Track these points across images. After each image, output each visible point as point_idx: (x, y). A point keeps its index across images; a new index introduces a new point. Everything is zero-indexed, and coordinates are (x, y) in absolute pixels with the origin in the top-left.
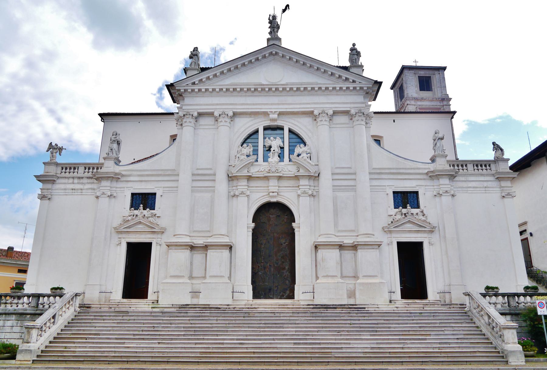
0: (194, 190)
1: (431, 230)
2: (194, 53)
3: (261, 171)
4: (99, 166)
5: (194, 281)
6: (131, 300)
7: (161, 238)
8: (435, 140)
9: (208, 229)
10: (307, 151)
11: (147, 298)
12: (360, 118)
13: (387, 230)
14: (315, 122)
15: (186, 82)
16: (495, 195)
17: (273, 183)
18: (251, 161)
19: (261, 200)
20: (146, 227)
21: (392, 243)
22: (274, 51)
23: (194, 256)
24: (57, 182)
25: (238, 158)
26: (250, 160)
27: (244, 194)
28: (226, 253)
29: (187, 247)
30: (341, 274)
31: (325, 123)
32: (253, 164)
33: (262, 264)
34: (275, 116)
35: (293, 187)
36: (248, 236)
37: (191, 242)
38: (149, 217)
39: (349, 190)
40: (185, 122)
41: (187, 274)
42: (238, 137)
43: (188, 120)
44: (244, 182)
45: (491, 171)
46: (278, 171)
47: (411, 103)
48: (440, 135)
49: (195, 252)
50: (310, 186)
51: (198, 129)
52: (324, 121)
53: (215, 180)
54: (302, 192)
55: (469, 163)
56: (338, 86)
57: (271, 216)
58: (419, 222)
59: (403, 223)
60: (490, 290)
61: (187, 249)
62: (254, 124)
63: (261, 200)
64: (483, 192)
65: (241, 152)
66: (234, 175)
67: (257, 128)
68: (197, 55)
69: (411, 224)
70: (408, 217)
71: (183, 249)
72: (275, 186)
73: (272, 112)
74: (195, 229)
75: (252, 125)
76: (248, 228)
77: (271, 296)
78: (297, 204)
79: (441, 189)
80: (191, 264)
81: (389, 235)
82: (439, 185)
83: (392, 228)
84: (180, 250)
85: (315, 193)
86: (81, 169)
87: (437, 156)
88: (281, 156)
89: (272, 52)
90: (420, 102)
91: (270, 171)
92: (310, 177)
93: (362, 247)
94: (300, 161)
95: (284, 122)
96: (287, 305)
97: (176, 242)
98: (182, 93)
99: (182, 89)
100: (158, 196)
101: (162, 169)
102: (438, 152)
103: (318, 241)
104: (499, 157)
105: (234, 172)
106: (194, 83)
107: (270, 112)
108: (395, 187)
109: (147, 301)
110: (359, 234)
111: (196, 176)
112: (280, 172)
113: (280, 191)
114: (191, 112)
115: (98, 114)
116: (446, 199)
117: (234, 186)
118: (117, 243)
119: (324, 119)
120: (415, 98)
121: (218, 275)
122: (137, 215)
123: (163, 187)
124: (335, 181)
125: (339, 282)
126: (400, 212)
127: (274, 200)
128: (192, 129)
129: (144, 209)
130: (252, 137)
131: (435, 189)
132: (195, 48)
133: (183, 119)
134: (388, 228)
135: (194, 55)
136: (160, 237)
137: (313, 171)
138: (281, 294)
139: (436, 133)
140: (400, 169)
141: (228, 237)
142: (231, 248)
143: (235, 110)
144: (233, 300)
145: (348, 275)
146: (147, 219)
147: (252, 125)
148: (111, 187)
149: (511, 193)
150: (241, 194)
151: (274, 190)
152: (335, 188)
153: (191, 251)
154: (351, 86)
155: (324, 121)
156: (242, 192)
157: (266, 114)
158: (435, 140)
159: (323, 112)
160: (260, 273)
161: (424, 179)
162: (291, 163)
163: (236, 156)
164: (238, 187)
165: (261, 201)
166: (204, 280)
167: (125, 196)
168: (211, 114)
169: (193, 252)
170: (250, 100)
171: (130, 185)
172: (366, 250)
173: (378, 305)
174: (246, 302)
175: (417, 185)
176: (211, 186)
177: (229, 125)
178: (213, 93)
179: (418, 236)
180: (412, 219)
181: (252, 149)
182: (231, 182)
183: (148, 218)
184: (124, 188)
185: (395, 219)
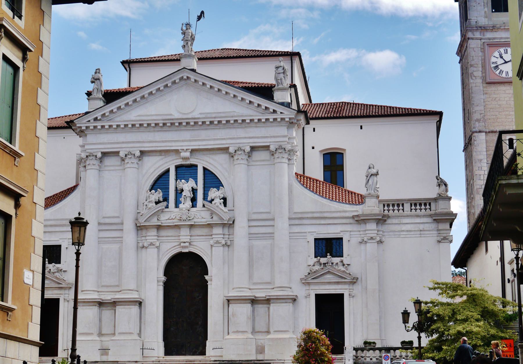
1: (352, 281)
3: (172, 219)
5: (103, 339)
6: (41, 358)
7: (69, 294)
8: (367, 177)
10: (220, 195)
11: (57, 356)
12: (281, 155)
13: (305, 282)
14: (232, 159)
18: (160, 208)
19: (172, 251)
20: (52, 282)
21: (309, 295)
23: (103, 312)
25: (146, 205)
27: (153, 245)
28: (135, 309)
29: (95, 304)
30: (253, 329)
31: (242, 162)
32: (164, 211)
33: (174, 319)
34: (188, 154)
35: (206, 236)
36: (159, 290)
37: (98, 299)
38: (55, 272)
39: (267, 238)
41: (95, 331)
42: (147, 180)
43: (92, 162)
45: (431, 211)
46: (190, 219)
47: (474, 35)
48: (374, 171)
49: (104, 308)
50: (224, 235)
51: (103, 170)
52: (241, 159)
53: (122, 230)
54: (215, 241)
55: (406, 202)
56: (256, 118)
57: (184, 267)
58: (339, 273)
59: (323, 274)
60: (367, 345)
61: (95, 306)
62: (165, 163)
63: (172, 251)
64: (418, 236)
65: (149, 199)
66: (142, 225)
67: (168, 168)
68: (99, 79)
69: (331, 275)
70: (328, 267)
71: (91, 306)
72: (187, 236)
73: (183, 149)
74: (103, 284)
75: (162, 165)
76: (158, 281)
77: (183, 353)
78: (210, 254)
79: (367, 235)
80: (100, 320)
81: (307, 288)
82: (365, 230)
83: (309, 280)
84: (88, 307)
85: (229, 243)
87: (367, 197)
88: (194, 200)
89: (183, 77)
90: (491, 33)
91: (181, 219)
92: (224, 225)
93: (274, 301)
94: (212, 207)
96: (194, 361)
97: (83, 299)
98: (84, 130)
99: (83, 126)
101: (66, 218)
102: (370, 191)
103: (229, 295)
104: (441, 194)
105: (142, 221)
106: (96, 119)
108: (317, 234)
109: (57, 358)
110: (275, 286)
112: (193, 219)
113: (192, 240)
114: (94, 152)
116: (371, 247)
117: (143, 236)
119: (240, 157)
120: (480, 27)
124: (251, 228)
125: (248, 338)
126: (318, 263)
127: (186, 250)
128: (96, 172)
130: (162, 177)
131: (361, 234)
133: (86, 160)
134: (305, 280)
135: (96, 79)
136: (68, 293)
137: (226, 218)
138: (194, 351)
139: (370, 168)
140: (324, 212)
141: (138, 293)
142: (140, 303)
143: (143, 149)
144: (143, 357)
146: (53, 274)
147: (162, 165)
149: (447, 238)
150: (150, 245)
151: (185, 241)
152: (252, 236)
153: (100, 307)
154: (271, 117)
155: (241, 157)
156: (151, 243)
157: (177, 152)
158: (367, 177)
160: (172, 329)
161: (350, 224)
162: (204, 209)
163: (143, 203)
164: (147, 238)
165: (173, 252)
169: (101, 308)
172: (279, 304)
173: (284, 360)
174: (157, 358)
176: (119, 236)
178: (117, 129)
179: (338, 288)
180: (331, 270)
181: (162, 195)
182: (139, 232)
183: (54, 273)
185: (312, 270)
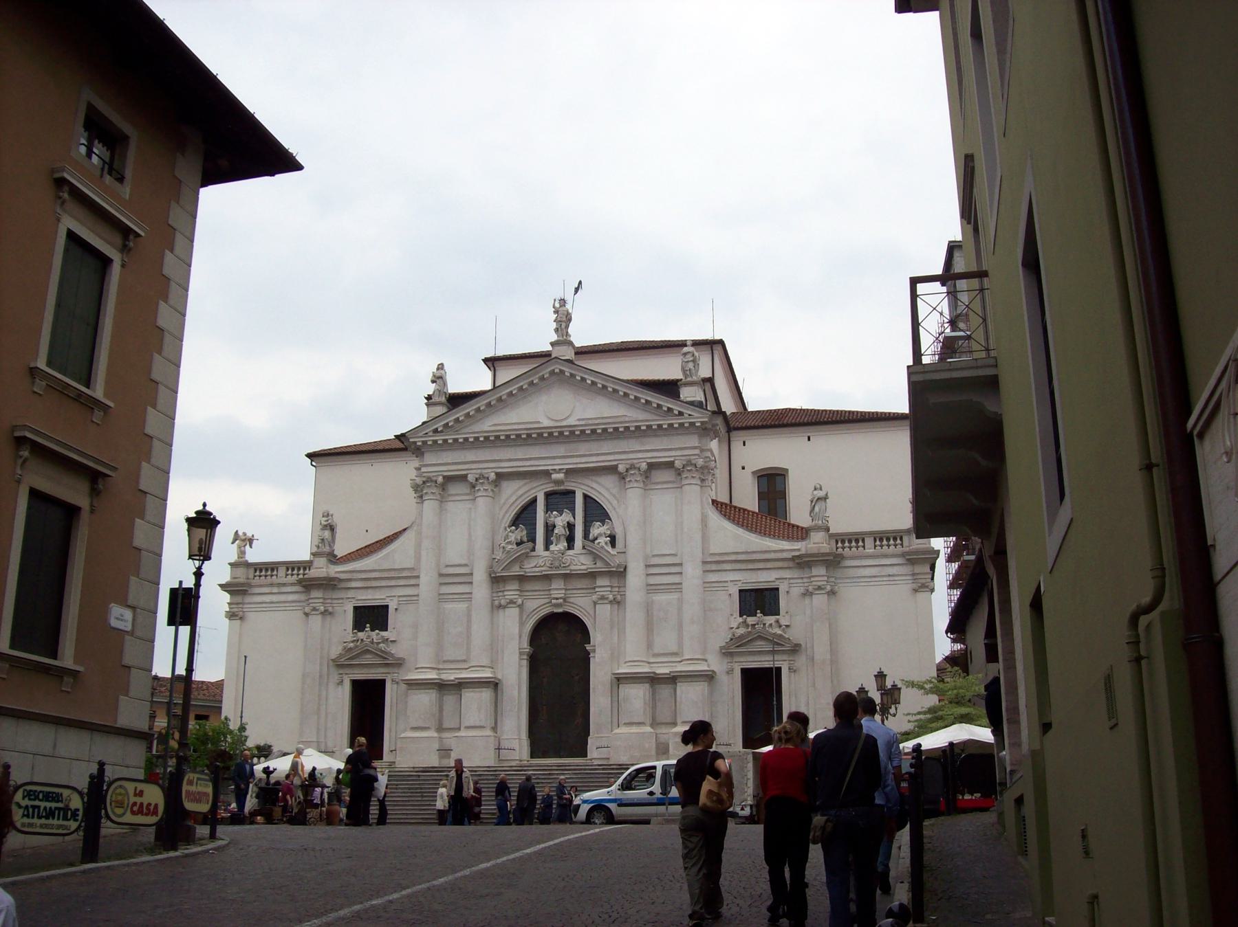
0: (442, 598)
2: (438, 374)
4: (306, 565)
9: (464, 658)
14: (623, 481)
15: (425, 430)
16: (903, 588)
17: (557, 585)
22: (556, 368)
24: (249, 592)
26: (522, 550)
28: (486, 695)
32: (529, 555)
40: (426, 493)
44: (515, 586)
49: (446, 692)
50: (612, 587)
66: (498, 575)
84: (423, 691)
86: (282, 571)
92: (610, 574)
95: (573, 484)
96: (566, 766)
100: (391, 610)
107: (552, 470)
111: (444, 578)
112: (569, 566)
115: (306, 455)
116: (820, 600)
118: (338, 681)
121: (477, 725)
122: (362, 640)
123: (399, 596)
129: (372, 630)
131: (804, 583)
132: (439, 365)
139: (815, 489)
142: (496, 685)
145: (664, 721)
148: (324, 599)
154: (676, 422)
157: (547, 474)
159: (632, 467)
166: (675, 727)
167: (345, 611)
168: (463, 478)
170: (520, 453)
171: (351, 594)
174: (518, 762)
175: (776, 579)
177: (491, 494)
184: (342, 599)
